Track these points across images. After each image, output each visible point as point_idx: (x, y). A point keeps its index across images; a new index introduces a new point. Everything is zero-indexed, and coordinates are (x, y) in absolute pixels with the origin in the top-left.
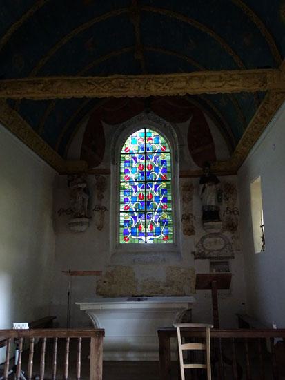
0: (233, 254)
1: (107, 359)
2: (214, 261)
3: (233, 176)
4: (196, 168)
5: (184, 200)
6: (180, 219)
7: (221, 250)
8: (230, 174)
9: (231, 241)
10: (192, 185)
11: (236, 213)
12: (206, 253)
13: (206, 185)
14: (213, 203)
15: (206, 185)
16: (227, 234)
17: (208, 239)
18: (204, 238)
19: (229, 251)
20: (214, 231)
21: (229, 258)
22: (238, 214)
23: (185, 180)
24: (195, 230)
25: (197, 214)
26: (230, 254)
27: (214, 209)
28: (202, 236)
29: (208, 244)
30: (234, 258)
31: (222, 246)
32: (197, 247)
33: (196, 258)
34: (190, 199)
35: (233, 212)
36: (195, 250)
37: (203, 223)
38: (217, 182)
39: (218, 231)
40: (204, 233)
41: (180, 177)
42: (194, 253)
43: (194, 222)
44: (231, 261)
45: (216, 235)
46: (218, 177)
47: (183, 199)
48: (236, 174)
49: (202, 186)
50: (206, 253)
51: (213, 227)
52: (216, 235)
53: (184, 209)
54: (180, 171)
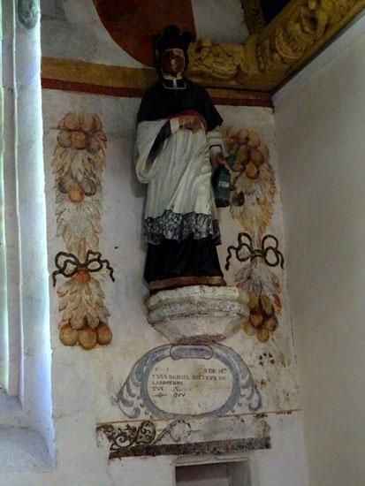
0: (266, 427)
1: (47, 56)
2: (189, 461)
3: (259, 109)
4: (111, 55)
5: (61, 187)
6: (46, 276)
7: (219, 413)
8: (248, 103)
9: (259, 373)
10: (95, 128)
11: (271, 257)
12: (161, 425)
13: (175, 124)
14: (204, 205)
15: (175, 124)
16: (244, 345)
17: (166, 367)
18: (151, 358)
19: (249, 420)
20: (202, 327)
21: (249, 445)
22: (280, 262)
23: (69, 102)
24: (111, 323)
25: (127, 257)
26: (251, 431)
27: (203, 229)
28: (142, 352)
29: (169, 389)
30: (268, 446)
31: (221, 398)
32: (119, 399)
33: (116, 454)
34: (91, 188)
35: (264, 254)
36: (115, 415)
37: (153, 292)
38: (213, 121)
39: (219, 329)
40: (151, 339)
41: (47, 83)
42: (105, 428)
43: (108, 287)
44: (258, 457)
45: (203, 344)
46: (219, 108)
47: (61, 187)
48: (268, 103)
49: (151, 130)
50: (161, 425)
51: (194, 311)
52: (203, 344)
53: (60, 227)
54: (44, 60)
